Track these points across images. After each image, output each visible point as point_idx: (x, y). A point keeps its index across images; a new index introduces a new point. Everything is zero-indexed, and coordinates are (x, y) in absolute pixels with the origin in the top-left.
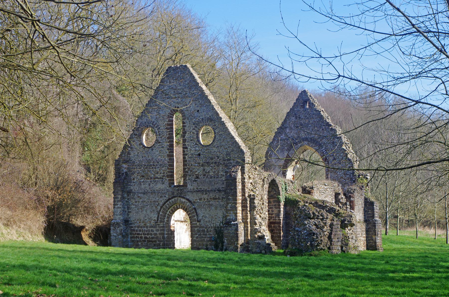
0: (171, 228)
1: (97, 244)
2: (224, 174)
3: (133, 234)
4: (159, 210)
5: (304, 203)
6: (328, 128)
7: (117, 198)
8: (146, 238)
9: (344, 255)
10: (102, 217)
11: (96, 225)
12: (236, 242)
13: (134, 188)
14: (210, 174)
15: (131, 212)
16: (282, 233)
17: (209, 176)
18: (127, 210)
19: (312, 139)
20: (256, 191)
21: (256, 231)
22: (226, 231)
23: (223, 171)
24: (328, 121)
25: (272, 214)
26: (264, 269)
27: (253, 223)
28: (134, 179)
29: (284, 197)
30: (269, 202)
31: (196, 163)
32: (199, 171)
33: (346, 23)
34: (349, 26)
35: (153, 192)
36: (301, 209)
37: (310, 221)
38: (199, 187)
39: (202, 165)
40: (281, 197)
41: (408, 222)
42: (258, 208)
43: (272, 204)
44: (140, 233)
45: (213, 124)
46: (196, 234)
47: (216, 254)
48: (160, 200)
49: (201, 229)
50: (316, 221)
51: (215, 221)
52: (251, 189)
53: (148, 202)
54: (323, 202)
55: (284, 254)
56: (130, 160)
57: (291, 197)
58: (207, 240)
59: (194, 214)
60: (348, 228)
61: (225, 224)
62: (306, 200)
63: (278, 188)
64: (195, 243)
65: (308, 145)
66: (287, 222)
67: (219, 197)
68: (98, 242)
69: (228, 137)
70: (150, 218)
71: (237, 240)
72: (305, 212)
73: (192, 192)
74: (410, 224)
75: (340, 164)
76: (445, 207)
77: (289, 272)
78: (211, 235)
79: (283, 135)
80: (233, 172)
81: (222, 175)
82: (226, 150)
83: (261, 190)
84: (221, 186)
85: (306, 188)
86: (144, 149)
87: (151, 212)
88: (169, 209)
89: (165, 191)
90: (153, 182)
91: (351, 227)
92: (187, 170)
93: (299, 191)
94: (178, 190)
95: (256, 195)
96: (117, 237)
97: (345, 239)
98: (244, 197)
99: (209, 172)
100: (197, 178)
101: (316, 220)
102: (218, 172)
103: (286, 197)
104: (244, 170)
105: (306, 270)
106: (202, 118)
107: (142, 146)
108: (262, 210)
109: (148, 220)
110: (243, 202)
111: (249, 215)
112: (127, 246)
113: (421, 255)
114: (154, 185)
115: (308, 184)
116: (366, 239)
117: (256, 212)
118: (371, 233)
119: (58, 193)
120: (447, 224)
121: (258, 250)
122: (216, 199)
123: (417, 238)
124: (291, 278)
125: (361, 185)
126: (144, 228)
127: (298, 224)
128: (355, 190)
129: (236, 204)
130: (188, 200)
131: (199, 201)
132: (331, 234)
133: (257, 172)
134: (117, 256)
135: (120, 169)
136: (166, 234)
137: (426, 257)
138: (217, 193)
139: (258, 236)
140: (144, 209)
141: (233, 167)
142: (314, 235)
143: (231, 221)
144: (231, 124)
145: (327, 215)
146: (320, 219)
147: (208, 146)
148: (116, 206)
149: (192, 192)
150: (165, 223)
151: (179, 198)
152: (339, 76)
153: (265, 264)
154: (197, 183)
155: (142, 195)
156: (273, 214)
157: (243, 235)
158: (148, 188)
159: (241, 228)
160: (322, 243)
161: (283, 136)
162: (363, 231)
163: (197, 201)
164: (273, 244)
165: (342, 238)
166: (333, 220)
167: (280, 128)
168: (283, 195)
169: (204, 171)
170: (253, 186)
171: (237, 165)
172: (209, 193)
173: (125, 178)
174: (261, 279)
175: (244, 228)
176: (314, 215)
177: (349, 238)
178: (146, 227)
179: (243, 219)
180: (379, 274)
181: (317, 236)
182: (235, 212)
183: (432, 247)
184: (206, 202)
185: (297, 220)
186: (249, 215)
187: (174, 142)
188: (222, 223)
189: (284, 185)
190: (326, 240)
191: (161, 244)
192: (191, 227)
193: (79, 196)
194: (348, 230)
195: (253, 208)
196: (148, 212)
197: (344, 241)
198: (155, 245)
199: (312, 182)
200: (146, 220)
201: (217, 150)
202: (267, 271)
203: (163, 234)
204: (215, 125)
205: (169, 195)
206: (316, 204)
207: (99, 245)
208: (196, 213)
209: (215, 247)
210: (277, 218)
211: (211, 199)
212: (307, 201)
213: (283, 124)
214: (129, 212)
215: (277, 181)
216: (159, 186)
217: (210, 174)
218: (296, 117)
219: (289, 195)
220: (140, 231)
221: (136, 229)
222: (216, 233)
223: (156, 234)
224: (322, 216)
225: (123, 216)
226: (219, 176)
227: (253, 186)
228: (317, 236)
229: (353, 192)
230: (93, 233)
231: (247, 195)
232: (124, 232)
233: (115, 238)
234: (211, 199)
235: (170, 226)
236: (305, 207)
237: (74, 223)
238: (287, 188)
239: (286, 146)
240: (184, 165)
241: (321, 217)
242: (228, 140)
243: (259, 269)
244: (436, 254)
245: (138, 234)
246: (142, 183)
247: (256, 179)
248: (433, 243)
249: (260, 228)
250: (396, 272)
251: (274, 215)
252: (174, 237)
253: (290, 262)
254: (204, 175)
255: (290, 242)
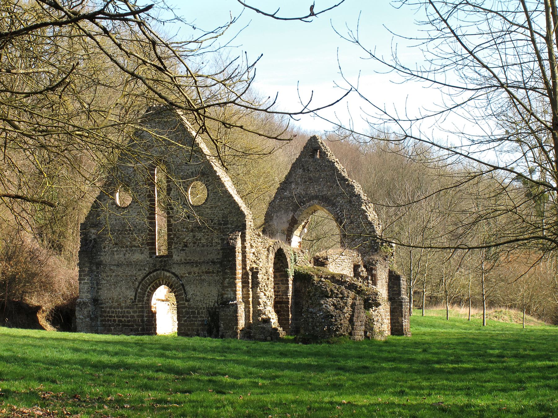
0: (152, 309)
1: (57, 328)
2: (220, 241)
3: (104, 317)
4: (137, 286)
5: (318, 277)
6: (344, 184)
7: (83, 271)
8: (120, 321)
9: (368, 341)
10: (63, 295)
11: (55, 305)
12: (235, 327)
13: (105, 258)
14: (202, 241)
15: (100, 289)
16: (291, 315)
17: (200, 244)
18: (96, 286)
19: (324, 197)
20: (260, 263)
21: (260, 312)
22: (222, 313)
23: (218, 238)
24: (343, 175)
25: (278, 292)
26: (285, 360)
27: (256, 302)
28: (105, 248)
29: (293, 270)
30: (275, 277)
31: (184, 228)
32: (188, 238)
33: (412, 74)
34: (415, 77)
35: (129, 264)
36: (316, 285)
37: (328, 300)
38: (188, 258)
39: (192, 231)
40: (289, 270)
41: (431, 298)
42: (262, 284)
43: (279, 278)
44: (113, 315)
45: (206, 179)
46: (185, 317)
47: (217, 343)
48: (138, 274)
49: (191, 310)
50: (335, 300)
51: (208, 301)
52: (253, 261)
53: (123, 276)
54: (342, 276)
55: (295, 341)
56: (99, 223)
57: (301, 271)
58: (198, 324)
59: (181, 292)
60: (372, 308)
61: (221, 304)
62: (320, 273)
63: (286, 259)
64: (183, 328)
65: (319, 204)
66: (297, 301)
67: (213, 271)
68: (57, 326)
69: (225, 195)
70: (125, 296)
71: (237, 324)
72: (321, 289)
73: (179, 264)
74: (434, 301)
75: (359, 228)
76: (482, 281)
77: (316, 363)
78: (203, 317)
79: (288, 192)
80: (231, 239)
81: (216, 243)
82: (222, 212)
83: (265, 261)
84: (214, 256)
85: (319, 258)
86: (117, 209)
87: (127, 289)
88: (149, 285)
89: (144, 262)
90: (129, 252)
91: (376, 307)
92: (172, 236)
93: (310, 263)
94: (161, 261)
95: (260, 268)
96: (84, 320)
97: (369, 322)
98: (244, 271)
99: (200, 239)
100: (186, 246)
101: (334, 298)
102: (212, 239)
103: (296, 270)
104: (245, 236)
105: (334, 361)
106: (191, 171)
107: (114, 206)
108: (267, 286)
109: (122, 299)
110: (244, 276)
111: (251, 292)
112: (97, 332)
113: (461, 341)
114: (130, 255)
115: (321, 254)
116: (391, 322)
117: (260, 289)
118: (396, 314)
119: (9, 264)
120: (484, 301)
121: (262, 336)
122: (209, 273)
123: (447, 319)
124: (323, 372)
125: (384, 254)
126: (118, 309)
127: (312, 304)
128: (377, 261)
129: (235, 279)
130: (173, 273)
131: (187, 275)
132: (352, 316)
133: (260, 239)
134: (100, 345)
135: (87, 235)
136: (146, 317)
137: (468, 343)
138: (211, 265)
139: (262, 319)
140: (118, 285)
141: (231, 233)
142: (332, 318)
143: (229, 300)
144: (228, 179)
145: (348, 293)
146: (340, 298)
147: (199, 206)
148: (83, 282)
149: (179, 264)
150: (144, 303)
151: (162, 272)
152: (407, 136)
153: (283, 354)
154: (186, 253)
155: (115, 268)
156: (279, 291)
157: (244, 319)
158: (122, 260)
159: (241, 309)
160: (343, 327)
161: (287, 193)
162: (387, 312)
163: (185, 275)
164: (280, 329)
165: (366, 321)
166: (355, 299)
167: (285, 182)
168: (292, 267)
169: (194, 238)
170: (256, 256)
171: (236, 231)
172: (201, 265)
173: (93, 247)
174: (287, 372)
175: (245, 309)
176: (332, 293)
177: (374, 321)
178: (121, 307)
179: (243, 298)
180: (422, 365)
181: (336, 319)
182: (234, 289)
183: (468, 330)
184: (196, 276)
185: (311, 299)
186: (251, 292)
187: (156, 201)
188: (217, 302)
189: (293, 255)
190: (346, 323)
191: (139, 329)
192: (178, 308)
193: (34, 269)
194: (373, 311)
195: (256, 284)
196: (123, 288)
197: (369, 325)
198: (132, 330)
199: (327, 251)
200: (121, 298)
201: (210, 212)
202: (289, 363)
203: (143, 316)
204: (209, 181)
205: (149, 268)
206: (332, 278)
207: (59, 330)
208: (185, 290)
209: (208, 333)
210: (284, 297)
211: (203, 272)
212: (322, 276)
213: (287, 178)
214: (98, 289)
215: (285, 251)
216: (137, 257)
217: (202, 241)
218: (304, 169)
219: (299, 268)
220: (113, 312)
221: (108, 310)
222: (210, 316)
223: (133, 317)
224: (341, 293)
225: (92, 293)
226: (214, 244)
227: (256, 256)
228: (336, 319)
229: (376, 263)
230: (52, 315)
231: (248, 268)
232: (92, 313)
233: (81, 321)
234: (203, 272)
235: (150, 307)
236: (321, 283)
237: (28, 302)
238: (297, 258)
239: (291, 206)
240: (169, 230)
241: (341, 296)
242: (225, 199)
243: (278, 360)
244: (477, 340)
245: (110, 317)
246: (115, 253)
247: (260, 248)
248: (466, 326)
249: (265, 308)
250: (441, 362)
251: (280, 293)
252: (155, 320)
253: (309, 351)
254: (195, 243)
255: (303, 326)
